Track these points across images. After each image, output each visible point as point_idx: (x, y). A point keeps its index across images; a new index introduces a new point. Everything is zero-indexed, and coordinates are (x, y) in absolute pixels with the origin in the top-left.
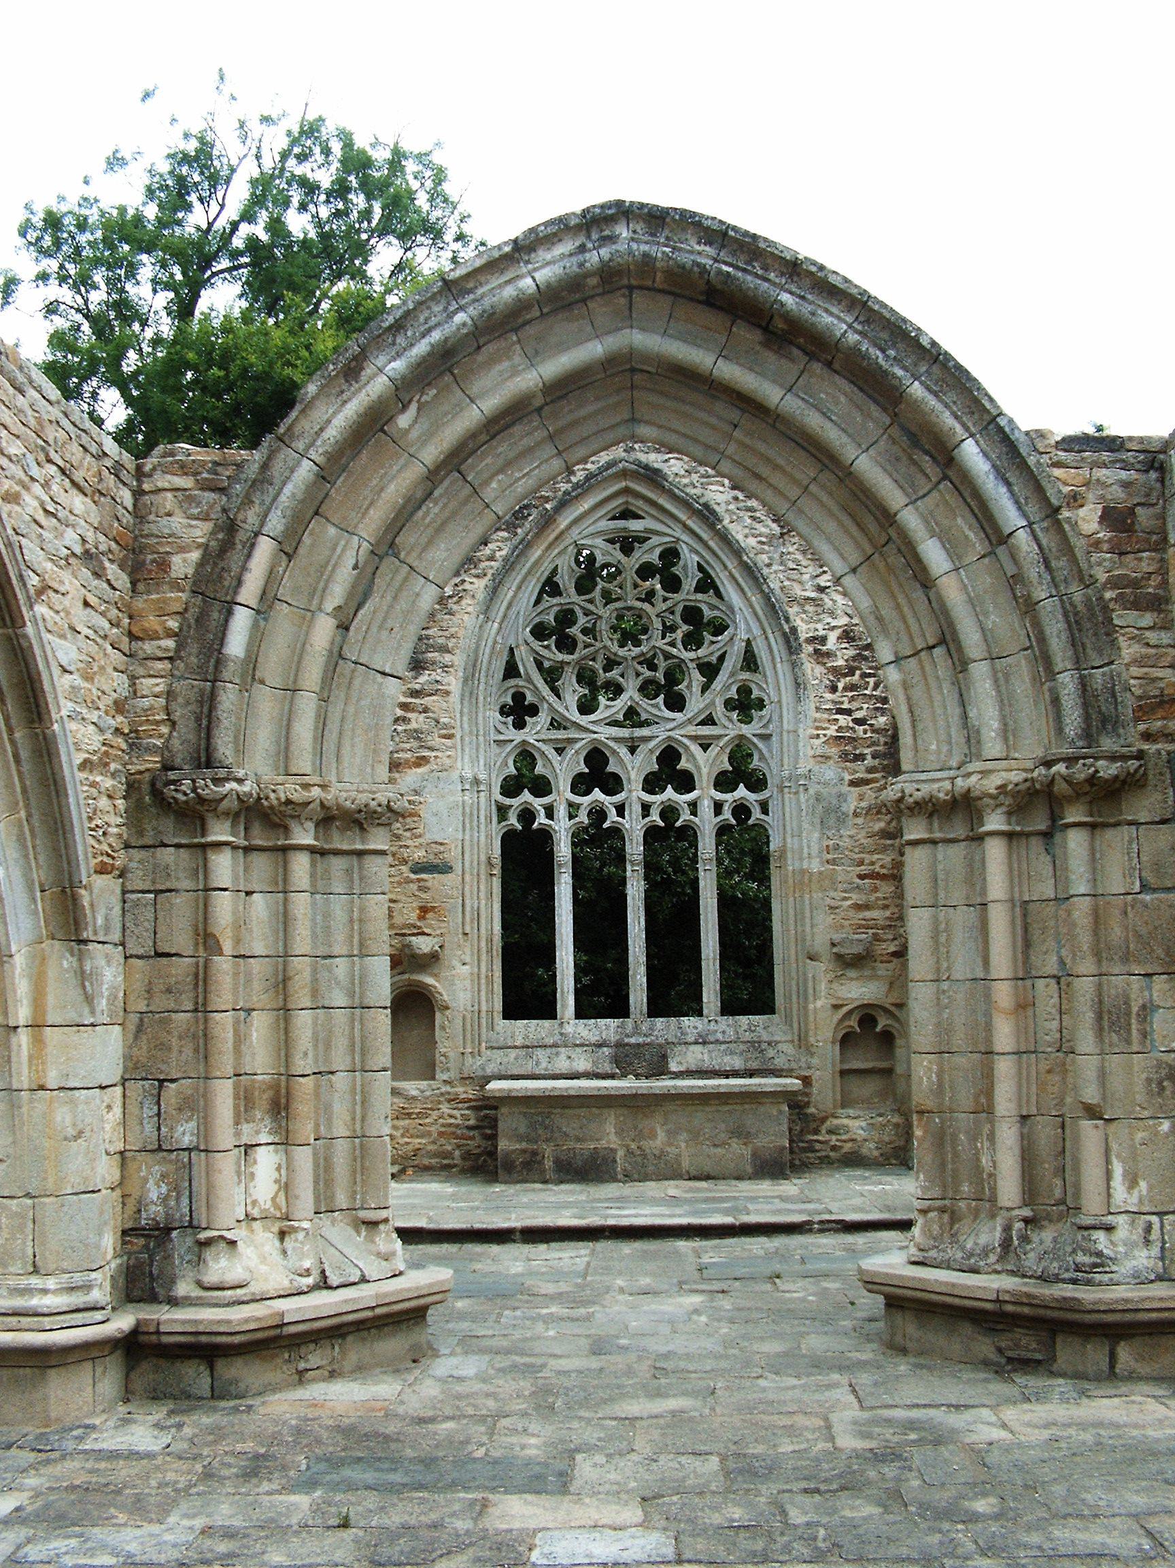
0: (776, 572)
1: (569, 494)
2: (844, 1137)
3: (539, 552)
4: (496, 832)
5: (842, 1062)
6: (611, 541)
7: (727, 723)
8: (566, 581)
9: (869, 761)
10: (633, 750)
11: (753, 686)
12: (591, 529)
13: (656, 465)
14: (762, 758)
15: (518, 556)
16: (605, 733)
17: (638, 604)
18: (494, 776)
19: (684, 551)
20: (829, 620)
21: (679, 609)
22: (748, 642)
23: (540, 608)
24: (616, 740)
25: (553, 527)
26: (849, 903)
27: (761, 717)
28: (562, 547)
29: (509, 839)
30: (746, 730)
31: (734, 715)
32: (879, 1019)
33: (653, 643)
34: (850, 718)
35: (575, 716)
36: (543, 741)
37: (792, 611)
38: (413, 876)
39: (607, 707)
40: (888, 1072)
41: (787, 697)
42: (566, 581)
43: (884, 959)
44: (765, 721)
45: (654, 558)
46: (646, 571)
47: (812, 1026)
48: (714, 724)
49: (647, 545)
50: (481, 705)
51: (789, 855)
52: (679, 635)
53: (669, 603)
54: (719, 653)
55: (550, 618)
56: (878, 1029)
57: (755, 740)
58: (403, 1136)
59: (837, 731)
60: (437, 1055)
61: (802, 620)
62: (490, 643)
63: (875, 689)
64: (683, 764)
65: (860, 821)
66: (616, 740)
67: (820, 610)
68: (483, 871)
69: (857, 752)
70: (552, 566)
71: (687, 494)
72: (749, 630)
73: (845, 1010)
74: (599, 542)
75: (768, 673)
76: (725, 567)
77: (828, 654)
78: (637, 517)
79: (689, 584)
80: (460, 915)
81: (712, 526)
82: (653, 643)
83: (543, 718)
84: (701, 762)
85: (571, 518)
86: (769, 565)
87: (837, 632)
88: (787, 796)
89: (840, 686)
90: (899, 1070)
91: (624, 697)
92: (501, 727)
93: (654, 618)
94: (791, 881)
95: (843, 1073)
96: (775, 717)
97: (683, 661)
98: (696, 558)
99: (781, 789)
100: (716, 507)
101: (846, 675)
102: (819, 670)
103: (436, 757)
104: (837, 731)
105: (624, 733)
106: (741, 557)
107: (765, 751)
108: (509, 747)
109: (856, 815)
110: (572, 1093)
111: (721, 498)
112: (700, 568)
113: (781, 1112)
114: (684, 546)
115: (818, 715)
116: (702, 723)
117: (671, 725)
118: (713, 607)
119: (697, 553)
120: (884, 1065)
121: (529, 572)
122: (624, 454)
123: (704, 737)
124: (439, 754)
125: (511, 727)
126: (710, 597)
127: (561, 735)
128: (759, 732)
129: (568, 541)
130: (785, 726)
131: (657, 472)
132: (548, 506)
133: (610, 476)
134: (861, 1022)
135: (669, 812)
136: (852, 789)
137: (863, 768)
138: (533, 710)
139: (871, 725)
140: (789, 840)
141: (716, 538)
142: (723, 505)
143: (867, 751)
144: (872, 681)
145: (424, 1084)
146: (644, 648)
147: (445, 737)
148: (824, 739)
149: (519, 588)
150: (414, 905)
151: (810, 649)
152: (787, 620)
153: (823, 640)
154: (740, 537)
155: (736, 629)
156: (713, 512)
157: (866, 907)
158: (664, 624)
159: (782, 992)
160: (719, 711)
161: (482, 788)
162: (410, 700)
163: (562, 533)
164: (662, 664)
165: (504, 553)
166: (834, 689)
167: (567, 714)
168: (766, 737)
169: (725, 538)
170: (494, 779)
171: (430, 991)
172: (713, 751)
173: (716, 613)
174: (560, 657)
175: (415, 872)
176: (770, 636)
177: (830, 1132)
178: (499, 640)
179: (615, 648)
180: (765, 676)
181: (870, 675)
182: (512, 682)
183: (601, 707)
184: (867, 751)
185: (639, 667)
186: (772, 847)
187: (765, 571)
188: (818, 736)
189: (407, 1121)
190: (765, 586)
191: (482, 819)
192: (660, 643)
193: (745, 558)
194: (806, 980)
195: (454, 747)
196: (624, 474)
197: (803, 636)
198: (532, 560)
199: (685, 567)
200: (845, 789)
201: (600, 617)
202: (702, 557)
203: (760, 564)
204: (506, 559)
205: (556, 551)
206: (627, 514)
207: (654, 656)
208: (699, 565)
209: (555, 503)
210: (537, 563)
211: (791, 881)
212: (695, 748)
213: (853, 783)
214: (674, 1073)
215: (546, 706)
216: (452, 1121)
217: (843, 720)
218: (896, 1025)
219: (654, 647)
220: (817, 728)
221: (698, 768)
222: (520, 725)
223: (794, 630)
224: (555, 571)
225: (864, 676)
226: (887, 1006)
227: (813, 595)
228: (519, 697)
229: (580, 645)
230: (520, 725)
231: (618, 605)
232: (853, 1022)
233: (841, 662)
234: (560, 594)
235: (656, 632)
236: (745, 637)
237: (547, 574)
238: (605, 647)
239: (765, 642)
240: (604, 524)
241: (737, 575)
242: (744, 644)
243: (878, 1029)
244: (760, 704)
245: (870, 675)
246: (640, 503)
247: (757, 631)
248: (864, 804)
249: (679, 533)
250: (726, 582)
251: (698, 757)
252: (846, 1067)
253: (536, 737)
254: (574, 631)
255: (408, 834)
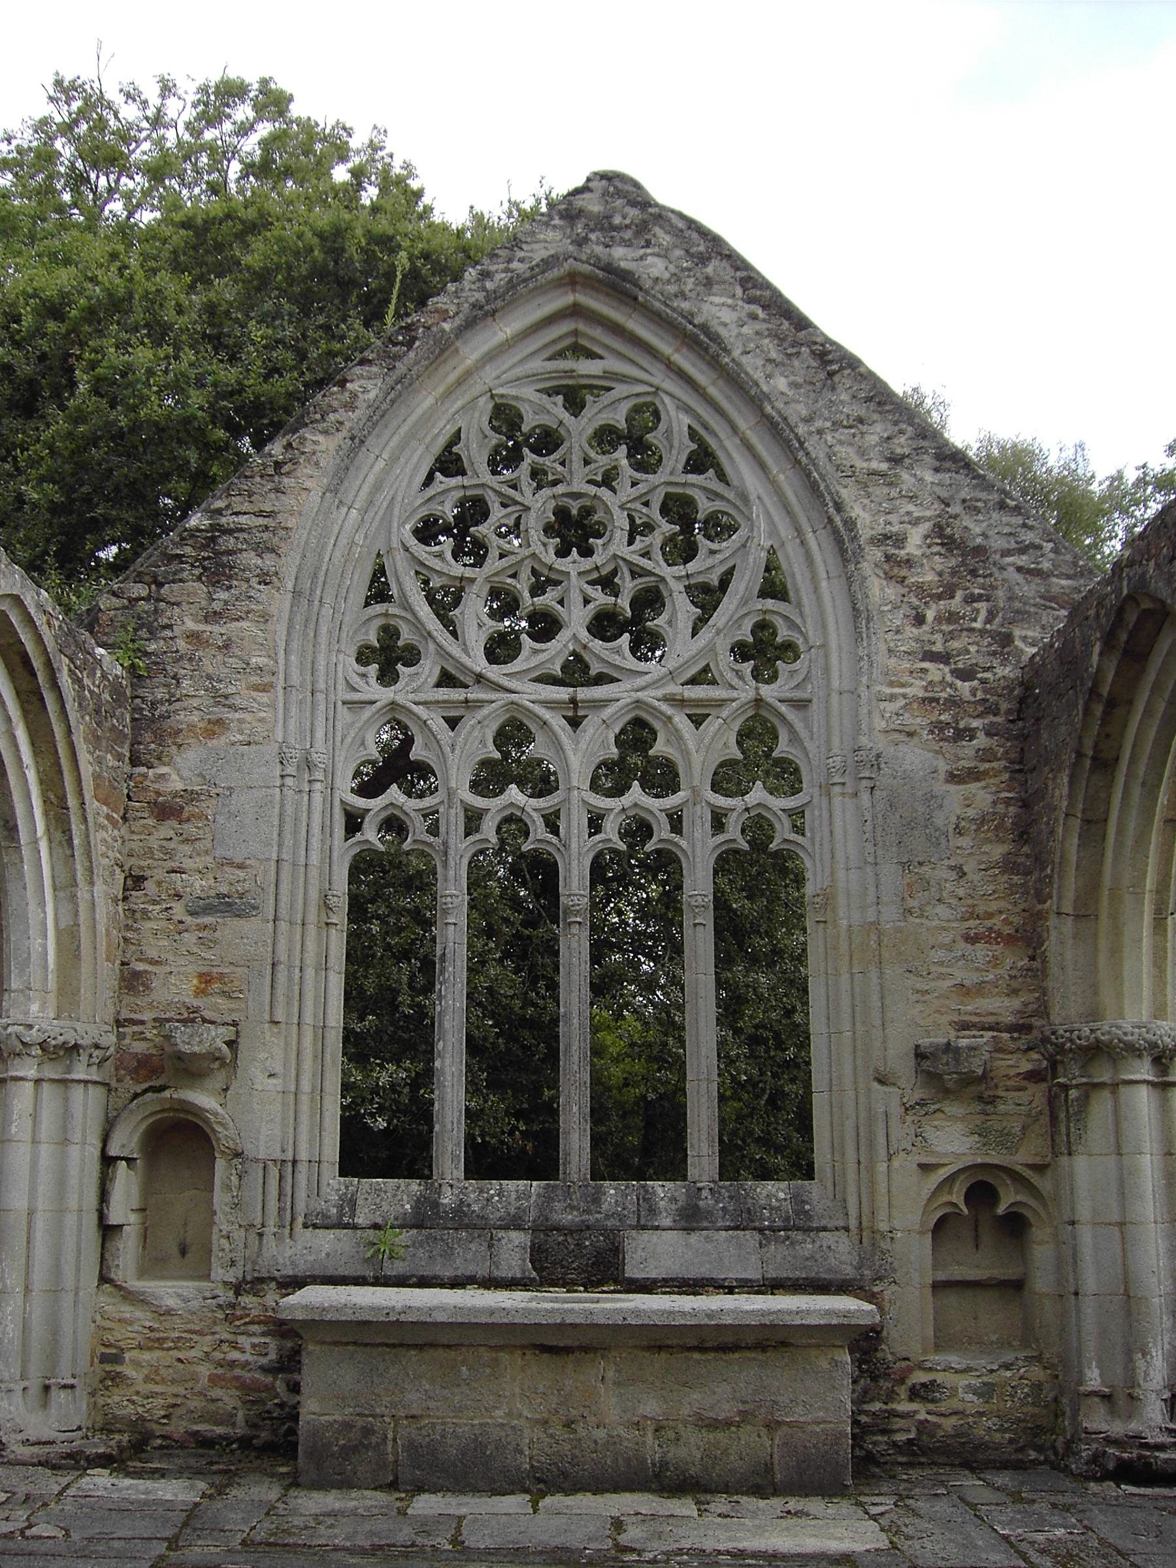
0: (820, 432)
1: (481, 308)
2: (943, 1407)
3: (430, 401)
4: (343, 853)
5: (935, 1267)
6: (550, 392)
7: (735, 682)
8: (475, 453)
9: (981, 741)
10: (575, 723)
11: (779, 622)
12: (518, 371)
13: (623, 264)
14: (795, 738)
15: (393, 402)
16: (530, 694)
17: (592, 490)
18: (340, 757)
19: (668, 407)
20: (911, 507)
21: (657, 501)
22: (772, 551)
23: (430, 491)
24: (548, 704)
25: (452, 363)
26: (949, 983)
27: (792, 673)
28: (467, 397)
29: (361, 865)
30: (767, 691)
31: (747, 667)
32: (1002, 1191)
33: (612, 549)
34: (947, 669)
35: (480, 663)
36: (424, 703)
37: (846, 494)
38: (188, 919)
39: (535, 652)
40: (1016, 1286)
41: (838, 635)
42: (475, 453)
43: (1010, 1083)
44: (799, 678)
45: (619, 418)
46: (606, 437)
47: (882, 1200)
48: (713, 682)
49: (607, 398)
50: (323, 640)
51: (841, 900)
52: (656, 540)
53: (642, 488)
54: (723, 568)
55: (449, 512)
56: (1001, 1210)
57: (783, 708)
58: (147, 1379)
59: (926, 689)
60: (215, 1237)
61: (864, 507)
62: (343, 541)
63: (988, 621)
64: (660, 748)
65: (965, 842)
66: (548, 704)
67: (894, 493)
68: (312, 917)
69: (962, 725)
70: (450, 430)
71: (674, 310)
72: (773, 531)
73: (943, 1173)
74: (529, 392)
75: (805, 600)
76: (734, 429)
77: (909, 562)
78: (592, 355)
79: (675, 459)
80: (268, 989)
81: (714, 363)
82: (612, 549)
83: (428, 669)
84: (691, 745)
85: (484, 349)
86: (808, 420)
87: (925, 527)
88: (837, 800)
89: (930, 615)
90: (1042, 1282)
91: (563, 636)
92: (356, 680)
93: (616, 512)
94: (844, 947)
95: (938, 1286)
96: (817, 672)
97: (663, 579)
98: (686, 420)
99: (826, 789)
100: (722, 332)
101: (939, 597)
102: (892, 592)
103: (241, 721)
104: (926, 689)
105: (562, 693)
106: (761, 409)
107: (799, 726)
108: (368, 712)
109: (959, 831)
110: (441, 1317)
111: (727, 316)
112: (693, 434)
113: (835, 1363)
114: (667, 399)
115: (892, 662)
116: (693, 681)
117: (640, 681)
118: (713, 495)
119: (688, 410)
120: (1009, 1272)
121: (412, 435)
122: (571, 248)
123: (698, 703)
124: (247, 716)
125: (373, 681)
126: (708, 479)
127: (457, 694)
128: (788, 695)
129: (478, 388)
130: (835, 684)
131: (626, 275)
132: (447, 326)
133: (549, 282)
134: (969, 1197)
135: (639, 830)
136: (953, 788)
137: (972, 753)
138: (412, 657)
139: (983, 681)
140: (841, 875)
141: (720, 382)
142: (733, 327)
143: (975, 724)
144: (983, 606)
145: (188, 1287)
146: (598, 559)
147: (257, 688)
148: (902, 702)
149: (394, 459)
150: (190, 969)
151: (875, 554)
152: (839, 507)
153: (899, 540)
154: (758, 375)
155: (752, 530)
156: (715, 338)
157: (980, 989)
158: (631, 519)
159: (826, 1144)
160: (724, 662)
161: (319, 775)
162: (201, 627)
163: (468, 374)
164: (629, 587)
165: (372, 396)
166: (920, 620)
167: (464, 659)
168: (801, 705)
169: (735, 380)
170: (339, 766)
171: (207, 1121)
172: (711, 726)
173: (719, 505)
174: (457, 569)
175: (192, 914)
176: (810, 536)
177: (915, 1394)
178: (359, 539)
179: (550, 557)
180: (799, 605)
181: (979, 598)
182: (379, 608)
183: (525, 652)
184: (975, 724)
185: (589, 590)
186: (809, 889)
187: (801, 430)
188: (892, 698)
189: (158, 1353)
190: (801, 454)
191: (316, 830)
192: (625, 551)
193: (768, 409)
194: (871, 1119)
195: (272, 706)
196: (573, 280)
197: (865, 534)
198: (419, 411)
199: (669, 433)
200: (940, 787)
201: (527, 509)
202: (698, 417)
203: (793, 420)
204: (374, 407)
205: (459, 404)
206: (579, 351)
207: (614, 572)
208: (691, 430)
209: (458, 321)
210: (428, 417)
211: (844, 947)
212: (681, 721)
213: (954, 778)
214: (632, 1281)
215: (432, 646)
216: (235, 1355)
217: (936, 671)
218: (1032, 1202)
219: (615, 556)
220: (891, 684)
221: (686, 753)
222: (387, 676)
223: (850, 524)
224: (456, 437)
225: (970, 599)
226: (1018, 1168)
227: (884, 466)
228: (389, 633)
229: (494, 553)
230: (387, 676)
231: (560, 489)
232: (957, 1197)
233: (930, 577)
234: (463, 473)
235: (618, 533)
236: (767, 544)
237: (441, 442)
238: (534, 555)
239: (801, 551)
240: (538, 365)
241: (754, 439)
242: (764, 554)
243: (1001, 1210)
244: (789, 650)
245: (979, 598)
246: (597, 332)
247: (785, 531)
248: (971, 813)
249: (659, 377)
250: (735, 455)
251: (687, 736)
252: (942, 1276)
253: (411, 696)
254: (483, 530)
255: (187, 849)
